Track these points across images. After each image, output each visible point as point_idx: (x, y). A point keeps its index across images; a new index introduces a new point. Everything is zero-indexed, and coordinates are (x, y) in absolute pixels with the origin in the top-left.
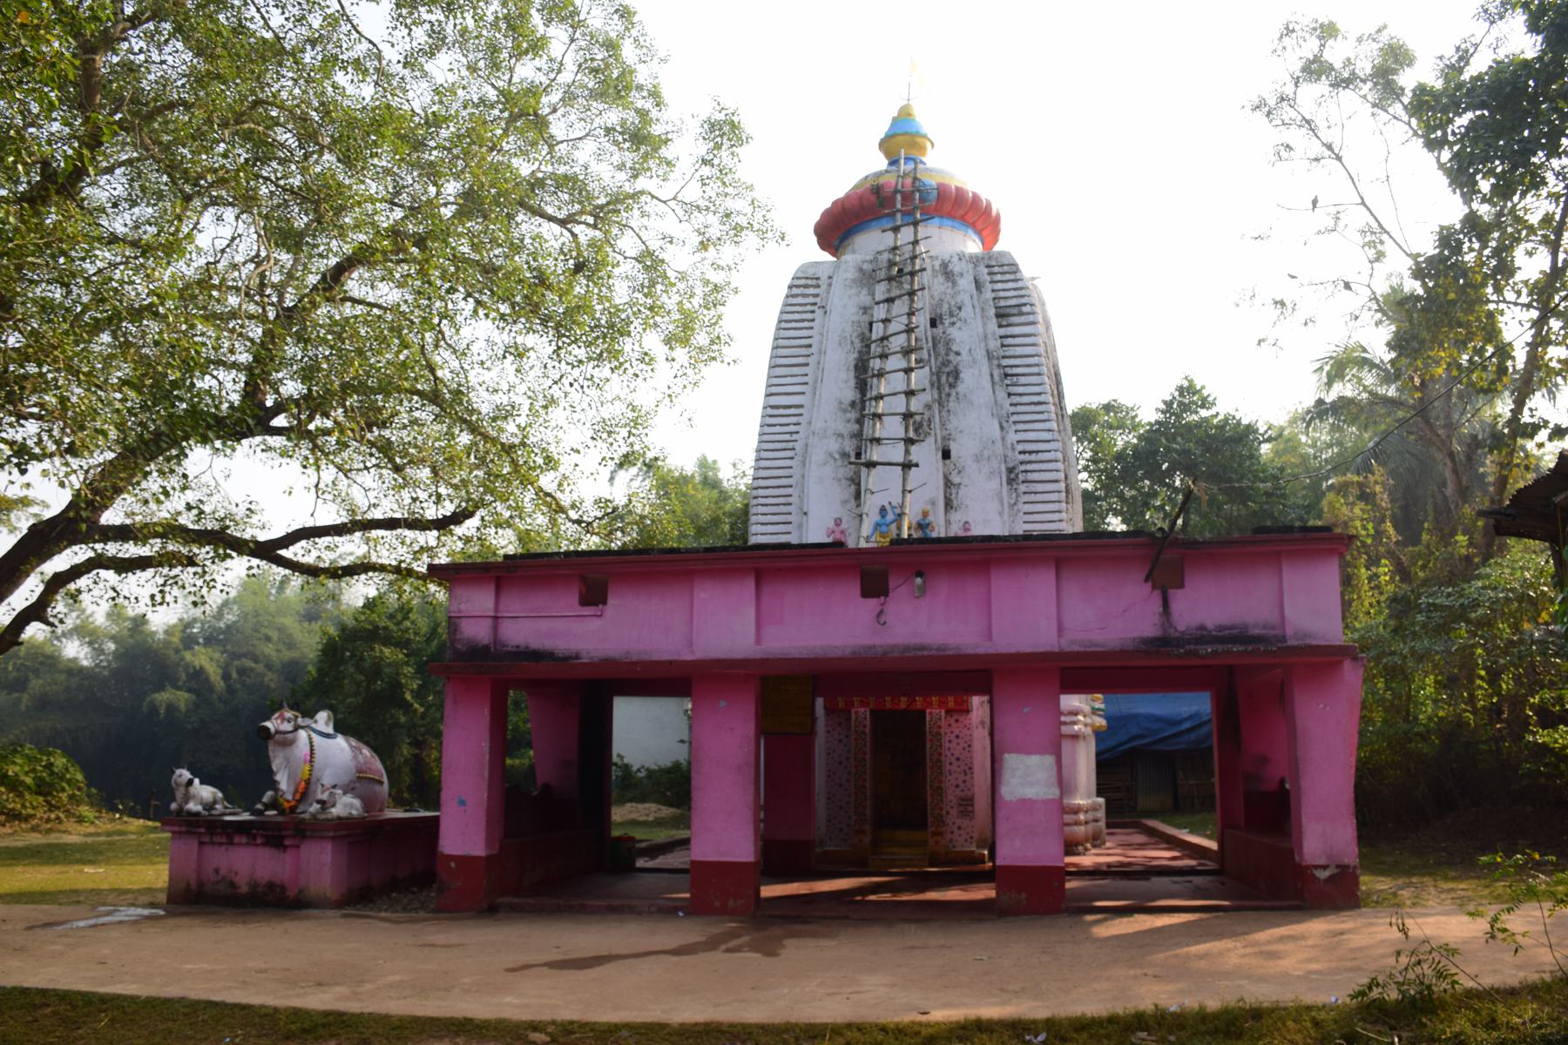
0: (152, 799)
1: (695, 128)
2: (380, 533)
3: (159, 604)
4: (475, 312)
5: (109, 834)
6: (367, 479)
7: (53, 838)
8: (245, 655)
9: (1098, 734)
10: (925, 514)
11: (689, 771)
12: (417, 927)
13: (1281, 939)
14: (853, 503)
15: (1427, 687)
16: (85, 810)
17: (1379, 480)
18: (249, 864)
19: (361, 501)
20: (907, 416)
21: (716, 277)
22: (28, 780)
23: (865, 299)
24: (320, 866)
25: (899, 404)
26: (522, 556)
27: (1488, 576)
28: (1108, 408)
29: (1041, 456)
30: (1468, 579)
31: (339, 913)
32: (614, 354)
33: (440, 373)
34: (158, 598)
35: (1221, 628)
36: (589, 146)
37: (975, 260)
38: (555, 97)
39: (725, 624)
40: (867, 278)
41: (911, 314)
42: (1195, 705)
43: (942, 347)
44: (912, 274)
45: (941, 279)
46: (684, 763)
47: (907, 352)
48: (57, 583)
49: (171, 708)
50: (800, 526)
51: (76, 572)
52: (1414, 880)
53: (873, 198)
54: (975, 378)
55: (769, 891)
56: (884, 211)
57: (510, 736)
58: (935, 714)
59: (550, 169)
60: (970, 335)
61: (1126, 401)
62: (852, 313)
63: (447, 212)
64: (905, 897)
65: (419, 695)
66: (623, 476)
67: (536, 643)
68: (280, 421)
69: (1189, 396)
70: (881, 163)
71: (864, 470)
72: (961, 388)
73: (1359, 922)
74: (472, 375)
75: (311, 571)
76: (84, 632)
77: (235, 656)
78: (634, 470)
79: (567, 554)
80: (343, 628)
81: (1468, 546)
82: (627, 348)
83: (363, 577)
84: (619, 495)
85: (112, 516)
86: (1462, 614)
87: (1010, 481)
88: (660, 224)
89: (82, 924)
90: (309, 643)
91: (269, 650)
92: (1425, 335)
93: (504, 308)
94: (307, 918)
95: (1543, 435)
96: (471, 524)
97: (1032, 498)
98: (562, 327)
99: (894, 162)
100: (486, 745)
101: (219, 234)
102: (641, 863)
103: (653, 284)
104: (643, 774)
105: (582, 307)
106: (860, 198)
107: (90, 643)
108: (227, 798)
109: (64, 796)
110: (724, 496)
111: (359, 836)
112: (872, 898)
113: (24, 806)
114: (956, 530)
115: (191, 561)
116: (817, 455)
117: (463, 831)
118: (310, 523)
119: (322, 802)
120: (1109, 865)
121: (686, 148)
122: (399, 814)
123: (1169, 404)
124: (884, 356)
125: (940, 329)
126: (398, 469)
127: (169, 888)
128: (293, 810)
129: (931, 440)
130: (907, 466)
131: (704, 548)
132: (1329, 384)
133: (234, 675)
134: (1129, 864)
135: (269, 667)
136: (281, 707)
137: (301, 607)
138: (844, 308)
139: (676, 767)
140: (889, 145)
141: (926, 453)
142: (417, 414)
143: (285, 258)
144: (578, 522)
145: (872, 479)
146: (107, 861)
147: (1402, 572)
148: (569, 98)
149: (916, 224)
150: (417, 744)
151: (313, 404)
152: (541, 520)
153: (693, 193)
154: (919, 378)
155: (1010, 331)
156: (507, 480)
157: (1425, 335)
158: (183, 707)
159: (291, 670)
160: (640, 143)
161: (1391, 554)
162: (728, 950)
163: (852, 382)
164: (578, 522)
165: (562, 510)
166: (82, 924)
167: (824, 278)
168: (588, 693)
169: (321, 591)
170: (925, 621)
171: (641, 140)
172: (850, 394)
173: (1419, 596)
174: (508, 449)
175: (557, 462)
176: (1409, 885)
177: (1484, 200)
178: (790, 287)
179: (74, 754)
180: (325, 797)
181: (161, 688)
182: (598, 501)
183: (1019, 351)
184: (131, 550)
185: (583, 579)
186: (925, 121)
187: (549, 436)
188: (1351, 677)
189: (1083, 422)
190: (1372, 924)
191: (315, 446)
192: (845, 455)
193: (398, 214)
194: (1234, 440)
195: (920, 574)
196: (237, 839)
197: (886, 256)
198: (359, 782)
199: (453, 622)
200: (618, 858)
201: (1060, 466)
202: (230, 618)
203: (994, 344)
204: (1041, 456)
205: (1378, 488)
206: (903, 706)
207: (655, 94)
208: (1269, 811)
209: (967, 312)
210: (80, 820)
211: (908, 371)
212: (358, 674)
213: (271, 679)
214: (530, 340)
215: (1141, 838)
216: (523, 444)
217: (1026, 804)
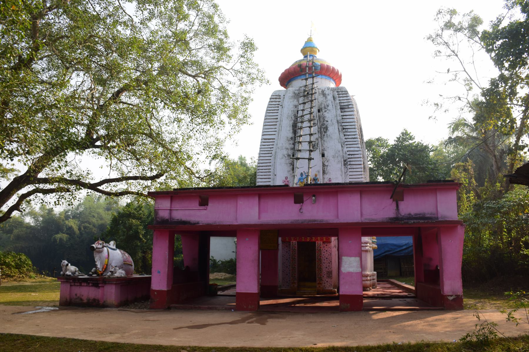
1: (239, 45)
2: (132, 181)
3: (57, 205)
4: (164, 107)
5: (40, 282)
6: (127, 163)
7: (21, 283)
8: (86, 222)
10: (316, 175)
12: (144, 314)
13: (436, 320)
14: (291, 172)
15: (486, 235)
16: (32, 274)
17: (470, 164)
18: (87, 293)
19: (125, 170)
20: (310, 142)
21: (246, 95)
22: (13, 264)
23: (296, 103)
24: (111, 293)
25: (307, 138)
26: (180, 189)
27: (507, 197)
28: (378, 140)
29: (355, 156)
32: (211, 121)
33: (152, 127)
34: (57, 203)
35: (416, 214)
37: (333, 90)
38: (191, 34)
39: (248, 212)
40: (296, 96)
41: (311, 108)
42: (407, 240)
44: (312, 94)
45: (322, 96)
47: (310, 121)
48: (23, 197)
49: (61, 239)
50: (274, 179)
51: (29, 194)
52: (482, 300)
53: (299, 69)
54: (333, 130)
57: (175, 250)
58: (319, 243)
59: (189, 58)
60: (331, 115)
61: (384, 137)
63: (155, 73)
65: (145, 236)
66: (214, 162)
67: (184, 219)
68: (98, 143)
69: (406, 136)
70: (301, 57)
71: (295, 161)
72: (328, 133)
73: (463, 314)
74: (163, 128)
76: (32, 214)
77: (83, 222)
78: (217, 160)
79: (195, 188)
80: (119, 213)
82: (215, 119)
83: (126, 196)
86: (498, 210)
87: (345, 165)
88: (227, 77)
89: (30, 312)
90: (108, 218)
91: (94, 220)
92: (486, 115)
93: (174, 106)
94: (107, 311)
96: (163, 178)
97: (352, 170)
98: (193, 112)
99: (306, 57)
100: (167, 253)
101: (78, 80)
102: (219, 293)
103: (224, 97)
104: (220, 263)
105: (200, 105)
106: (294, 68)
107: (34, 218)
108: (80, 270)
109: (25, 269)
110: (248, 169)
112: (297, 305)
113: (11, 272)
114: (326, 181)
115: (68, 190)
117: (159, 282)
118: (108, 178)
120: (378, 295)
121: (235, 52)
122: (138, 276)
123: (399, 138)
124: (302, 122)
125: (321, 113)
126: (138, 160)
129: (318, 150)
130: (310, 159)
132: (453, 132)
133: (82, 229)
135: (94, 226)
136: (98, 240)
137: (105, 206)
138: (288, 106)
139: (231, 260)
140: (304, 51)
141: (316, 155)
142: (144, 141)
143: (100, 88)
144: (199, 178)
145: (298, 164)
146: (39, 291)
147: (478, 196)
148: (196, 35)
149: (313, 77)
150: (144, 252)
151: (109, 137)
152: (186, 177)
153: (238, 67)
154: (314, 130)
156: (175, 163)
157: (486, 115)
158: (65, 239)
159: (102, 227)
161: (474, 190)
162: (248, 323)
163: (291, 131)
164: (199, 178)
165: (193, 174)
166: (30, 312)
167: (282, 96)
168: (202, 235)
170: (316, 212)
171: (220, 49)
172: (291, 135)
173: (484, 204)
174: (175, 153)
175: (192, 157)
176: (480, 302)
177: (506, 70)
178: (270, 99)
179: (28, 255)
180: (113, 270)
182: (205, 171)
183: (348, 120)
184: (48, 186)
185: (200, 197)
186: (316, 43)
188: (461, 231)
189: (370, 144)
192: (289, 155)
193: (138, 74)
194: (421, 151)
195: (314, 196)
196: (76, 284)
197: (303, 88)
198: (124, 265)
200: (211, 291)
201: (362, 159)
202: (81, 209)
203: (339, 118)
204: (355, 156)
205: (470, 167)
206: (308, 240)
207: (225, 34)
208: (432, 276)
210: (30, 277)
211: (310, 127)
212: (124, 229)
213: (95, 230)
214: (183, 116)
215: (389, 286)
216: (180, 151)
217: (350, 274)
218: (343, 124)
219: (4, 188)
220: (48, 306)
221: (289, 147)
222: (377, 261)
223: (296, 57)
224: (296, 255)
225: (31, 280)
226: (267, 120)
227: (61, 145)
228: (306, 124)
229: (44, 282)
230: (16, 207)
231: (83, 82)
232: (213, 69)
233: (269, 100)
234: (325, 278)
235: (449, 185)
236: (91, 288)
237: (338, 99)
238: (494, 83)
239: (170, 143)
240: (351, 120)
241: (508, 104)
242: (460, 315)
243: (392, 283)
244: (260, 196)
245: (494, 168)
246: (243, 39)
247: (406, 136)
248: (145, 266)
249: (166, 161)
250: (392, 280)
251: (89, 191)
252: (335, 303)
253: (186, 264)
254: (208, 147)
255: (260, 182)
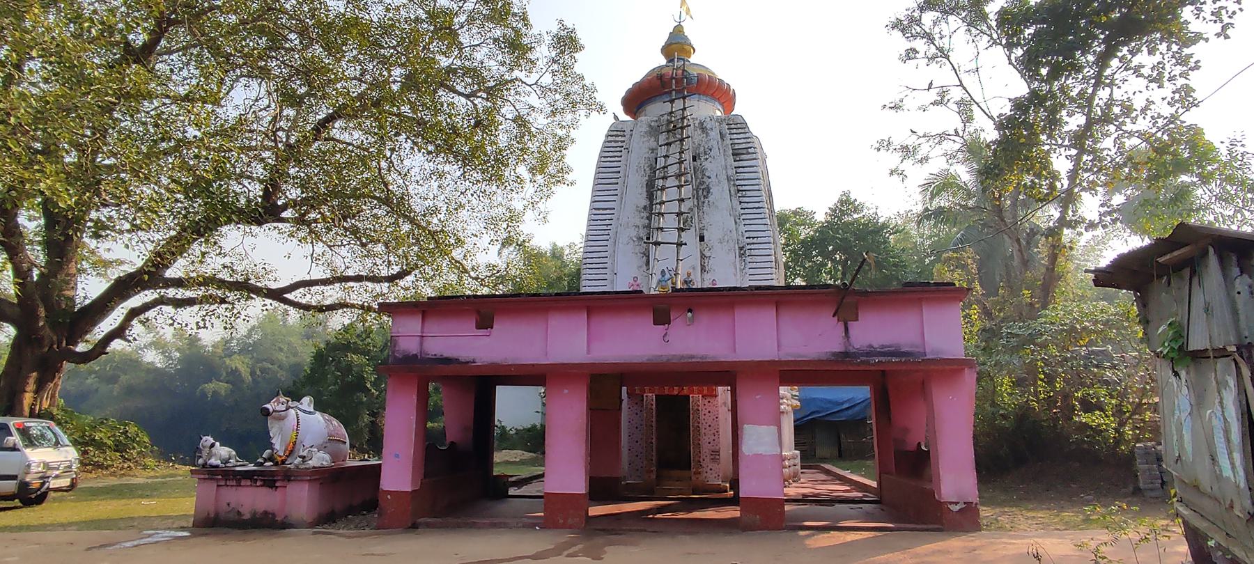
1: (548, 39)
2: (352, 284)
3: (211, 330)
5: (164, 477)
6: (344, 251)
7: (125, 481)
8: (265, 360)
9: (795, 411)
10: (689, 275)
12: (363, 540)
13: (934, 553)
14: (645, 268)
15: (1005, 383)
16: (149, 461)
17: (969, 255)
18: (252, 499)
19: (339, 263)
20: (679, 214)
21: (560, 132)
22: (109, 443)
23: (653, 144)
24: (300, 500)
25: (674, 207)
26: (439, 298)
27: (1046, 316)
28: (795, 213)
29: (759, 240)
32: (500, 178)
34: (201, 324)
35: (883, 346)
37: (720, 121)
38: (463, 18)
39: (568, 341)
40: (654, 131)
42: (862, 393)
43: (699, 173)
44: (682, 128)
45: (700, 132)
48: (134, 313)
50: (612, 282)
51: (146, 307)
54: (720, 193)
55: (595, 511)
56: (673, 89)
57: (433, 409)
58: (695, 398)
59: (459, 63)
60: (717, 166)
61: (807, 208)
63: (395, 87)
65: (374, 384)
66: (505, 251)
68: (287, 214)
69: (846, 204)
70: (663, 61)
72: (711, 198)
73: (984, 541)
74: (410, 188)
75: (307, 308)
76: (158, 345)
77: (259, 361)
78: (511, 249)
79: (468, 297)
80: (328, 343)
81: (1031, 297)
82: (507, 174)
85: (175, 271)
86: (1031, 339)
87: (741, 255)
88: (529, 97)
89: (128, 544)
90: (306, 355)
91: (281, 356)
92: (1003, 165)
93: (431, 148)
94: (289, 535)
96: (410, 278)
97: (754, 265)
99: (670, 60)
100: (413, 418)
101: (244, 97)
102: (512, 491)
103: (522, 136)
104: (513, 432)
105: (479, 148)
106: (650, 81)
107: (162, 353)
108: (239, 454)
109: (134, 452)
110: (564, 265)
111: (330, 478)
112: (659, 516)
113: (105, 459)
114: (707, 285)
115: (223, 301)
116: (623, 239)
117: (398, 473)
118: (308, 278)
120: (804, 495)
121: (543, 53)
123: (834, 211)
124: (665, 178)
125: (698, 162)
126: (363, 245)
127: (195, 516)
128: (283, 462)
129: (693, 229)
130: (679, 245)
131: (550, 294)
132: (932, 199)
133: (258, 372)
136: (278, 394)
138: (640, 148)
140: (667, 50)
141: (690, 237)
142: (375, 211)
143: (291, 113)
144: (476, 279)
145: (656, 253)
147: (987, 313)
149: (684, 98)
150: (373, 414)
151: (311, 202)
152: (453, 277)
153: (547, 80)
154: (686, 192)
155: (741, 164)
156: (431, 253)
158: (223, 393)
159: (295, 369)
161: (978, 302)
162: (569, 556)
164: (476, 279)
165: (465, 271)
166: (128, 544)
168: (481, 385)
170: (693, 340)
171: (516, 47)
172: (644, 202)
173: (1001, 328)
174: (433, 234)
175: (463, 242)
178: (607, 136)
179: (144, 424)
180: (305, 454)
183: (747, 176)
184: (181, 293)
185: (478, 312)
186: (691, 32)
188: (969, 377)
189: (782, 219)
191: (311, 232)
192: (640, 239)
193: (364, 86)
194: (872, 232)
195: (690, 311)
196: (243, 483)
199: (393, 340)
200: (497, 489)
202: (256, 337)
203: (731, 172)
204: (759, 240)
205: (970, 261)
206: (676, 393)
207: (525, 19)
208: (915, 463)
210: (145, 467)
211: (680, 187)
212: (336, 378)
214: (447, 168)
215: (823, 477)
216: (442, 231)
218: (738, 183)
219: (94, 297)
221: (640, 224)
222: (799, 429)
223: (648, 60)
225: (145, 473)
226: (601, 175)
227: (211, 213)
228: (671, 182)
229: (175, 476)
230: (119, 333)
231: (257, 100)
232: (502, 83)
234: (707, 463)
237: (729, 137)
238: (1020, 105)
239: (424, 216)
241: (1044, 144)
242: (977, 543)
243: (828, 472)
245: (1016, 262)
247: (846, 204)
248: (373, 441)
250: (827, 466)
251: (268, 301)
253: (451, 436)
255: (588, 285)
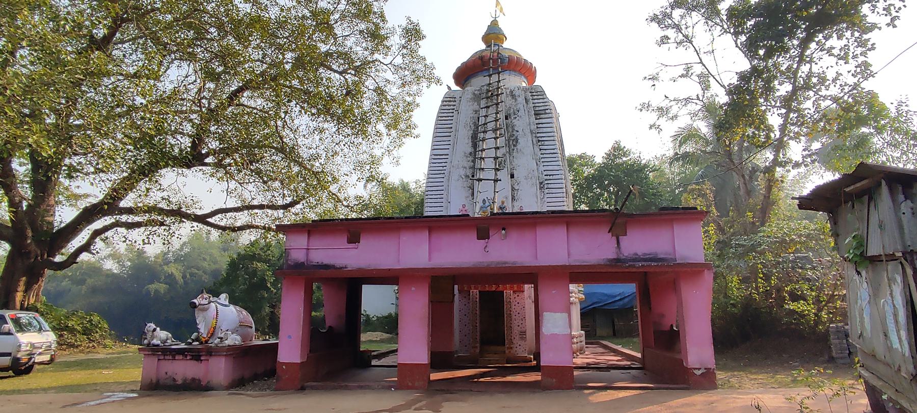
0: (138, 336)
1: (399, 31)
2: (256, 211)
3: (153, 245)
4: (300, 111)
6: (250, 187)
7: (90, 356)
9: (581, 302)
10: (503, 203)
11: (397, 315)
12: (265, 399)
13: (683, 406)
15: (734, 281)
16: (108, 342)
18: (183, 369)
19: (247, 195)
20: (496, 158)
21: (409, 99)
22: (79, 328)
23: (476, 107)
24: (219, 369)
25: (492, 153)
26: (320, 221)
27: (764, 231)
28: (581, 157)
29: (554, 177)
30: (756, 233)
31: (227, 392)
32: (364, 132)
33: (285, 140)
34: (146, 241)
35: (645, 254)
36: (353, 39)
37: (525, 90)
38: (337, 16)
39: (415, 252)
40: (477, 98)
41: (497, 113)
42: (630, 288)
43: (510, 128)
44: (498, 95)
46: (394, 314)
47: (495, 130)
48: (97, 233)
49: (156, 291)
50: (447, 208)
51: (106, 229)
52: (736, 373)
53: (480, 62)
54: (525, 142)
55: (435, 376)
56: (490, 66)
57: (319, 300)
58: (508, 293)
59: (334, 49)
60: (523, 123)
61: (589, 153)
62: (470, 113)
63: (288, 67)
64: (510, 378)
65: (274, 284)
66: (369, 186)
67: (326, 261)
69: (617, 150)
70: (483, 46)
71: (476, 183)
72: (519, 146)
74: (299, 140)
75: (224, 229)
76: (114, 256)
79: (342, 220)
80: (239, 254)
83: (248, 231)
84: (365, 195)
85: (127, 202)
86: (753, 248)
87: (541, 188)
88: (386, 73)
89: (92, 403)
90: (223, 262)
91: (205, 264)
92: (732, 121)
93: (314, 111)
94: (210, 396)
95: (789, 167)
96: (299, 206)
98: (339, 120)
99: (489, 46)
100: (302, 309)
101: (177, 75)
104: (375, 318)
106: (474, 61)
107: (118, 262)
108: (173, 337)
109: (97, 335)
110: (412, 196)
113: (76, 341)
114: (516, 210)
115: (162, 224)
116: (455, 177)
117: (291, 350)
119: (221, 338)
120: (588, 364)
121: (395, 41)
122: (260, 342)
123: (609, 155)
124: (485, 132)
126: (265, 182)
128: (206, 342)
130: (496, 181)
132: (680, 146)
133: (188, 276)
134: (598, 364)
135: (205, 272)
136: (202, 292)
137: (220, 245)
138: (467, 110)
139: (390, 315)
140: (486, 38)
141: (503, 175)
142: (273, 157)
143: (212, 86)
144: (348, 206)
146: (115, 368)
147: (720, 229)
148: (343, 17)
149: (499, 73)
150: (273, 307)
151: (226, 151)
153: (399, 60)
154: (501, 142)
155: (541, 121)
156: (314, 188)
157: (732, 121)
159: (215, 273)
160: (375, 38)
161: (714, 221)
163: (470, 144)
164: (348, 206)
165: (340, 201)
166: (92, 403)
167: (458, 97)
168: (351, 285)
169: (229, 237)
170: (507, 251)
171: (376, 37)
172: (470, 149)
174: (316, 174)
175: (338, 180)
176: (734, 376)
177: (760, 59)
178: (443, 101)
179: (104, 315)
180: (222, 336)
181: (152, 282)
182: (356, 197)
184: (131, 219)
185: (349, 231)
187: (335, 168)
188: (708, 276)
189: (571, 162)
190: (726, 398)
191: (227, 173)
192: (467, 176)
193: (265, 66)
195: (504, 229)
197: (485, 87)
198: (242, 327)
200: (363, 361)
201: (564, 181)
202: (186, 250)
203: (534, 127)
205: (708, 191)
207: (382, 16)
208: (669, 340)
209: (522, 111)
210: (105, 346)
211: (496, 138)
212: (245, 280)
213: (206, 278)
214: (326, 125)
215: (601, 350)
216: (323, 172)
217: (554, 336)
218: (539, 135)
220: (122, 391)
222: (584, 314)
224: (478, 321)
227: (153, 160)
228: (490, 134)
232: (366, 63)
233: (440, 103)
234: (517, 341)
235: (677, 214)
236: (189, 362)
240: (549, 130)
242: (715, 398)
243: (605, 347)
244: (430, 230)
245: (742, 192)
246: (404, 24)
247: (617, 150)
249: (303, 185)
251: (195, 224)
252: (534, 377)
253: (329, 323)
254: (359, 165)
